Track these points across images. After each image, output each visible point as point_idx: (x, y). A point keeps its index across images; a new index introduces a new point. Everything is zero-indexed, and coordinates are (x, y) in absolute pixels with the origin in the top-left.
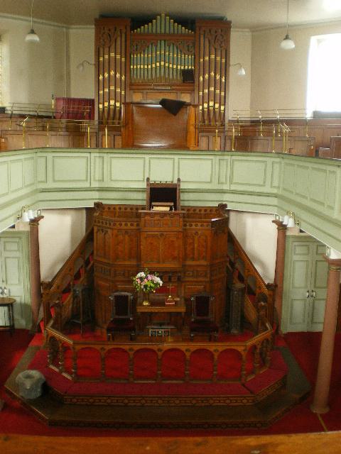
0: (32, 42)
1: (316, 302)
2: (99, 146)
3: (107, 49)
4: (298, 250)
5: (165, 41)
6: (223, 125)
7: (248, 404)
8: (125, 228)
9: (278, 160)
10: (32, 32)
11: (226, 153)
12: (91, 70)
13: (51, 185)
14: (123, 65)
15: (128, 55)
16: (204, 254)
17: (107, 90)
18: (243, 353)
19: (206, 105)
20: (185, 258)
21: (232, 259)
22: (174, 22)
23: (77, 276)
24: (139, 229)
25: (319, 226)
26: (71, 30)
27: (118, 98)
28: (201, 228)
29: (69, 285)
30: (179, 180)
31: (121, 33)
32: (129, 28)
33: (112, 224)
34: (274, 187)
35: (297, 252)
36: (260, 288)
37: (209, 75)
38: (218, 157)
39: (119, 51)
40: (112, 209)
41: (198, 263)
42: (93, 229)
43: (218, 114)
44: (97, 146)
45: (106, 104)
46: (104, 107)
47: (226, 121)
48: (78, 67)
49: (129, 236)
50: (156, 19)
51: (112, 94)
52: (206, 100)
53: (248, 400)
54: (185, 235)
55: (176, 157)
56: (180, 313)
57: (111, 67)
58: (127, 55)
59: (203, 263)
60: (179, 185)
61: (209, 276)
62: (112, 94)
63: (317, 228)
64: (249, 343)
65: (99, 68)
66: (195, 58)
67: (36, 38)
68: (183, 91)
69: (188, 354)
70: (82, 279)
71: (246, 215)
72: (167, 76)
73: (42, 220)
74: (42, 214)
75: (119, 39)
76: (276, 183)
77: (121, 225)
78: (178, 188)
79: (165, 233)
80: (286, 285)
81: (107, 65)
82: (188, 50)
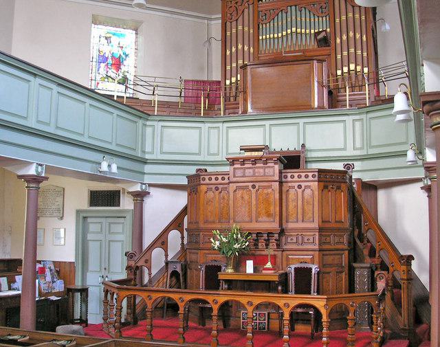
5: (296, 6)
18: (323, 312)
34: (357, 149)
35: (120, 244)
46: (231, 83)
52: (346, 62)
55: (301, 121)
57: (238, 41)
63: (107, 217)
75: (246, 10)
76: (358, 145)
78: (302, 155)
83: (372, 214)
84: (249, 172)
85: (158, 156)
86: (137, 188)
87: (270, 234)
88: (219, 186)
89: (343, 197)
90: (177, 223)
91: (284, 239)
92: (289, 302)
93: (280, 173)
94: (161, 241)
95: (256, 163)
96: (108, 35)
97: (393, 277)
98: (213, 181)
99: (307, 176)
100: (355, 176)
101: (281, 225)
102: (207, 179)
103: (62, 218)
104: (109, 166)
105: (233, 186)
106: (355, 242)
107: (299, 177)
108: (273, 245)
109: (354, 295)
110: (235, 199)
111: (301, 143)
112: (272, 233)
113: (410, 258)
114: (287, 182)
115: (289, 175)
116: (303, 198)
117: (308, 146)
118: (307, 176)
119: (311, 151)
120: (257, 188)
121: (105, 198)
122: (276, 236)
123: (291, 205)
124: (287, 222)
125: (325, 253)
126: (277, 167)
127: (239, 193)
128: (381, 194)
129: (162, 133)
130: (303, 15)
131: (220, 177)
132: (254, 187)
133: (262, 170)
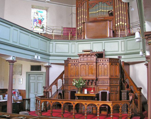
5: (101, 2)
18: (111, 107)
34: (123, 51)
35: (41, 84)
46: (79, 28)
52: (119, 21)
55: (103, 42)
56: (94, 96)
57: (82, 14)
61: (109, 83)
63: (37, 74)
75: (84, 4)
76: (123, 50)
78: (104, 53)
83: (128, 73)
84: (85, 59)
85: (54, 53)
86: (47, 64)
87: (93, 80)
88: (75, 64)
89: (118, 68)
90: (61, 77)
91: (97, 82)
92: (99, 103)
93: (96, 59)
94: (55, 83)
95: (88, 56)
96: (37, 12)
97: (135, 95)
98: (73, 62)
99: (105, 60)
100: (122, 60)
101: (96, 77)
103: (21, 75)
104: (38, 57)
105: (80, 64)
106: (122, 83)
107: (103, 61)
108: (94, 84)
109: (121, 101)
110: (81, 68)
111: (103, 49)
112: (93, 80)
113: (141, 88)
114: (98, 62)
115: (99, 60)
116: (104, 68)
117: (106, 50)
118: (105, 60)
119: (107, 52)
120: (88, 64)
121: (36, 68)
122: (95, 81)
123: (100, 70)
124: (99, 76)
125: (111, 87)
126: (95, 57)
127: (82, 66)
128: (131, 67)
129: (55, 46)
130: (104, 5)
131: (75, 61)
132: (87, 64)
133: (90, 58)
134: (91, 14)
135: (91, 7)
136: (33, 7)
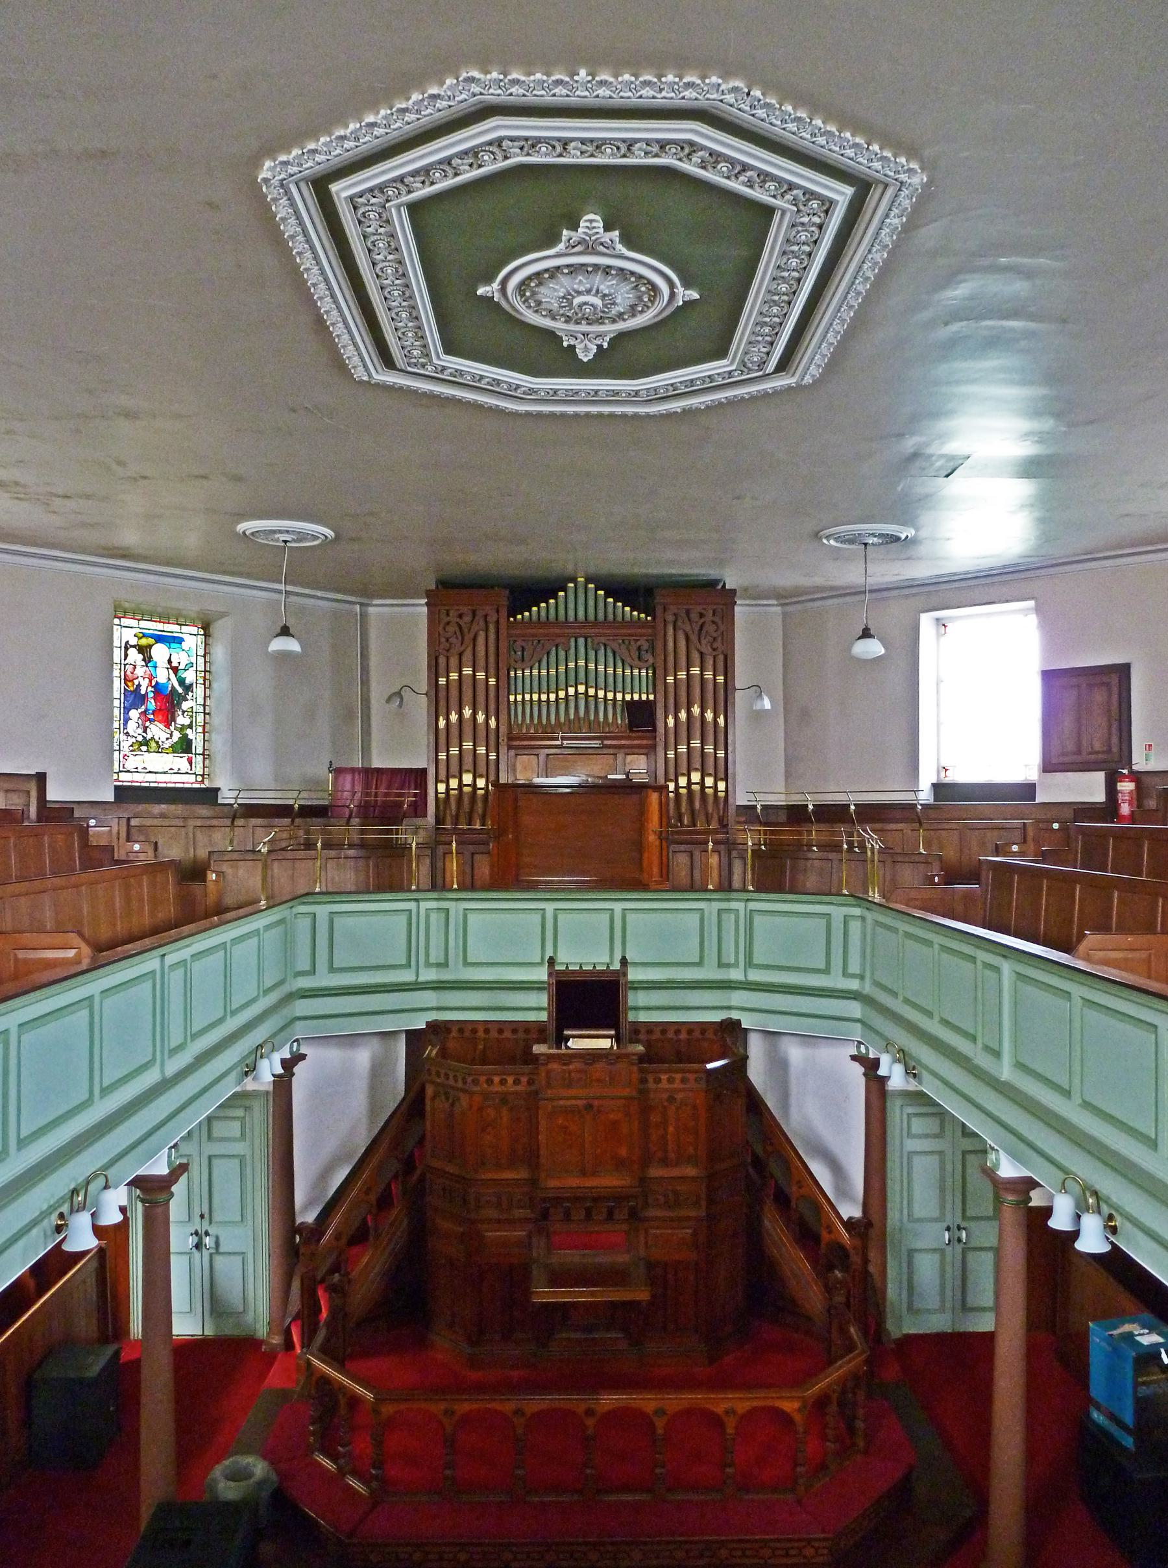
0: (284, 657)
1: (970, 1256)
2: (438, 884)
3: (454, 661)
4: (918, 1125)
6: (723, 824)
7: (820, 1559)
8: (499, 1089)
9: (857, 911)
10: (285, 631)
11: (734, 895)
12: (420, 706)
13: (325, 980)
14: (492, 694)
15: (503, 672)
16: (691, 1150)
17: (454, 751)
18: (797, 1418)
19: (683, 781)
20: (646, 1161)
21: (759, 1149)
22: (607, 596)
23: (384, 1202)
24: (537, 1092)
25: (973, 1095)
26: (371, 610)
27: (482, 769)
28: (682, 1086)
29: (364, 1222)
30: (624, 962)
31: (486, 622)
32: (504, 612)
33: (469, 1079)
34: (853, 976)
36: (830, 1228)
37: (689, 712)
38: (716, 906)
39: (481, 662)
40: (467, 1034)
41: (675, 1172)
42: (422, 1090)
43: (711, 800)
44: (434, 887)
45: (454, 783)
47: (732, 810)
48: (388, 700)
49: (511, 1109)
50: (564, 589)
51: (468, 761)
53: (817, 1549)
54: (643, 1104)
56: (639, 1303)
58: (500, 669)
59: (690, 1171)
60: (625, 974)
61: (703, 1203)
62: (468, 761)
64: (816, 1389)
65: (439, 701)
66: (654, 673)
67: (291, 645)
68: (631, 750)
69: (660, 1424)
70: (395, 1212)
71: (785, 1039)
72: (592, 717)
73: (301, 1064)
74: (303, 1051)
76: (854, 967)
77: (490, 1082)
79: (596, 1103)
80: (894, 1216)
81: (454, 693)
82: (639, 658)
83: (879, 1285)
96: (144, 642)
102: (664, 1082)
115: (664, 1077)
119: (636, 1009)
130: (601, 659)
134: (553, 709)
135: (519, 664)
136: (121, 611)
